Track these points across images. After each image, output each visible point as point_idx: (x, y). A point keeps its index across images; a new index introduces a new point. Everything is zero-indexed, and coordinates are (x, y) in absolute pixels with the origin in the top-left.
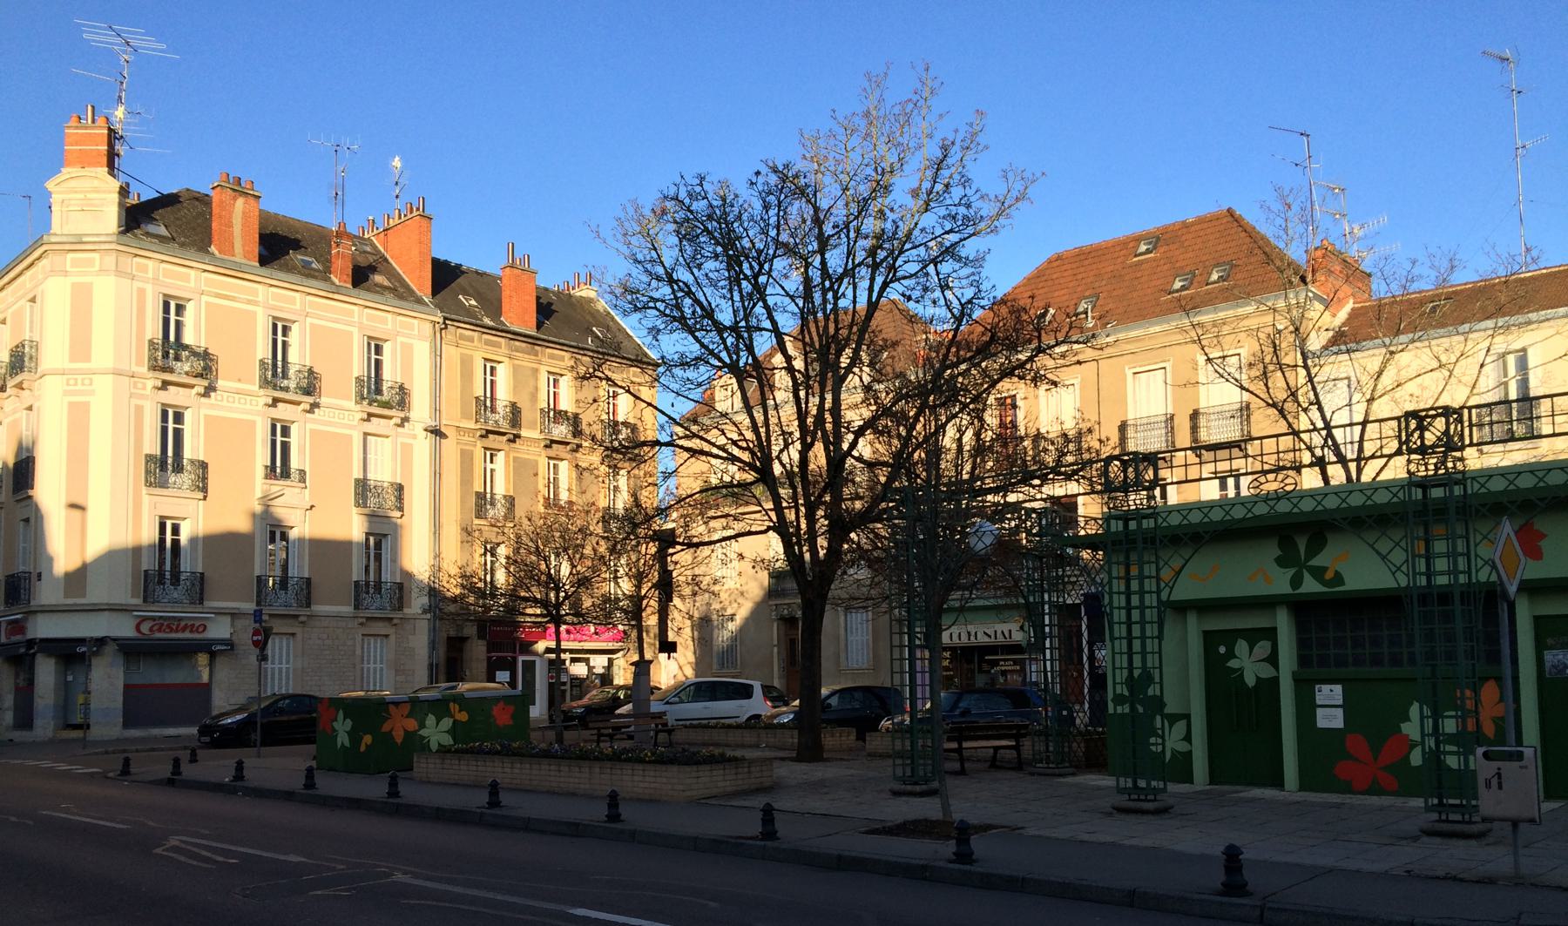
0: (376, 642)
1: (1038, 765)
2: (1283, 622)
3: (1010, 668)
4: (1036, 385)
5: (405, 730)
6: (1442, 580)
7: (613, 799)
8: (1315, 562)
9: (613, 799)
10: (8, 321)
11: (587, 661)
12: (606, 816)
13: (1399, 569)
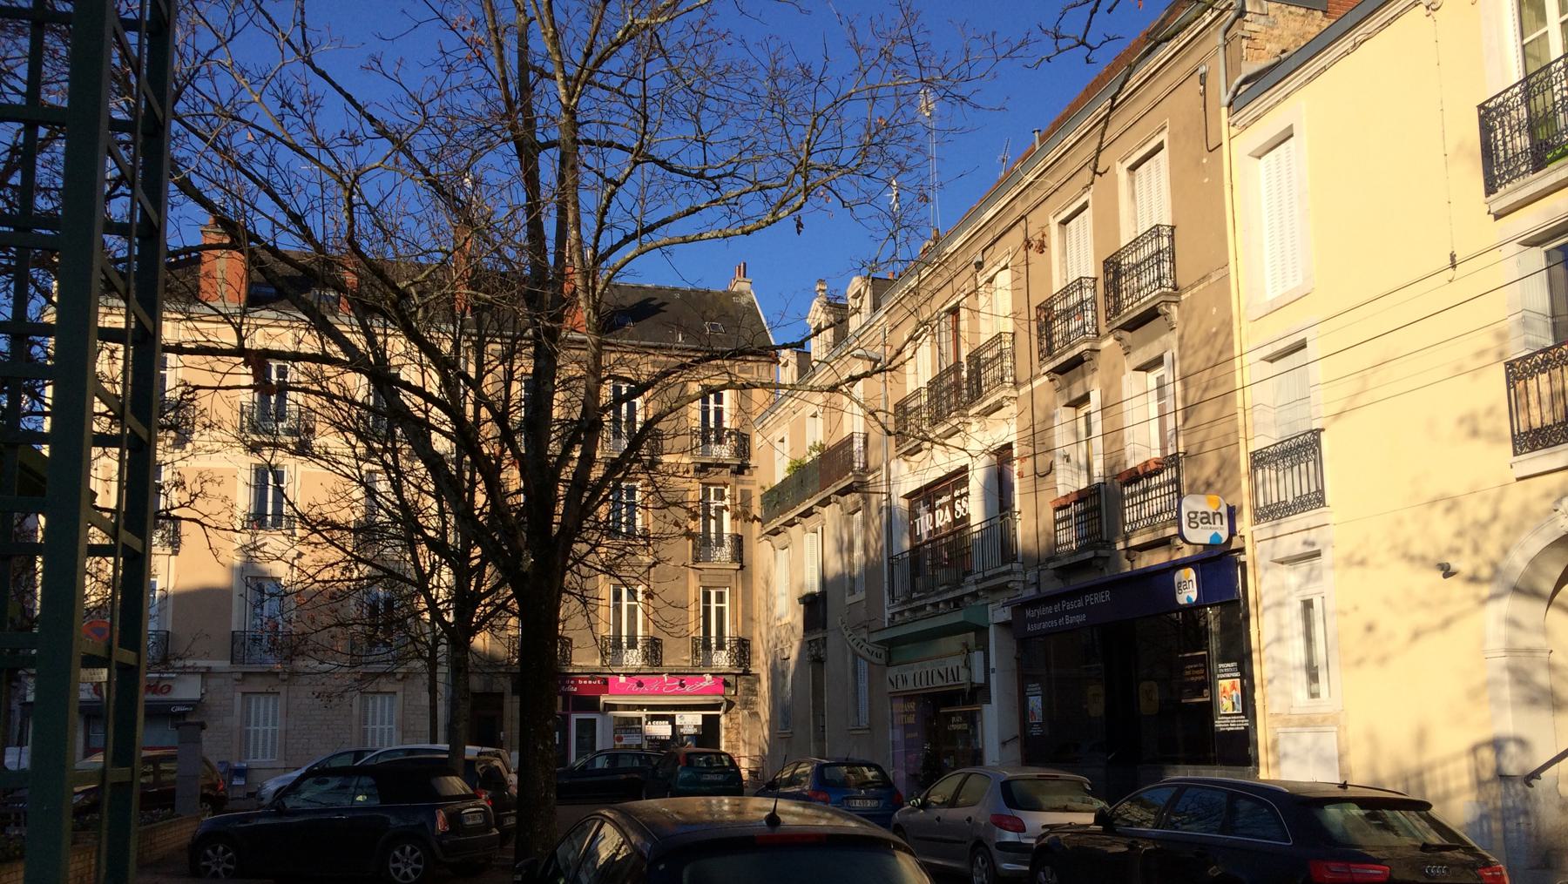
0: (383, 701)
4: (664, 304)
10: (786, 440)
11: (672, 720)
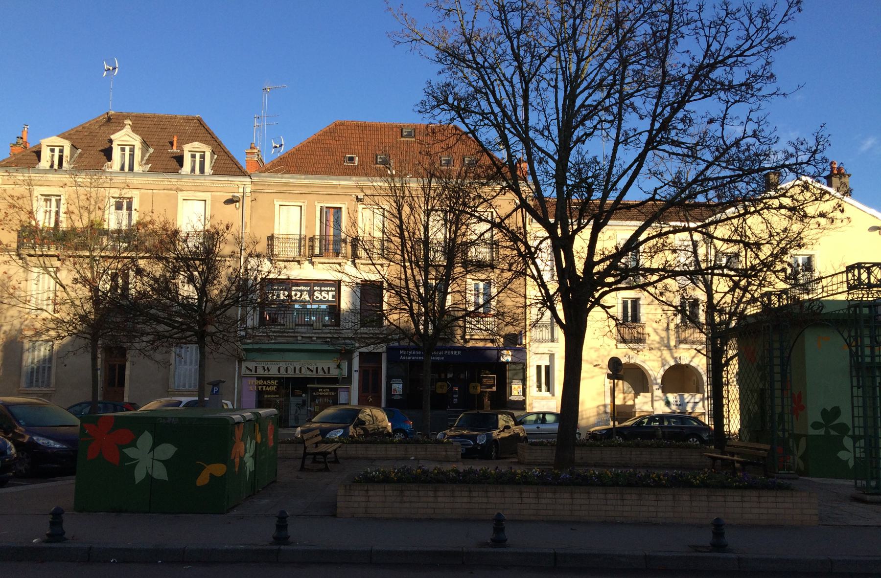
3: (326, 394)
5: (137, 447)
9: (718, 528)
12: (274, 538)
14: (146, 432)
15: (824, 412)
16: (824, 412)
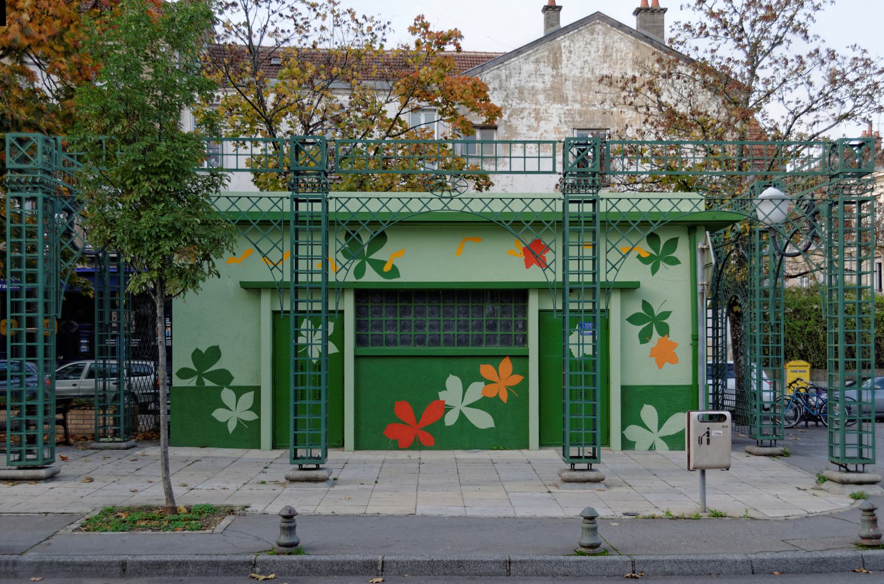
1: (102, 440)
2: (348, 305)
6: (573, 278)
7: (289, 517)
8: (374, 256)
13: (275, 266)
14: (214, 414)
15: (197, 355)
16: (197, 355)
